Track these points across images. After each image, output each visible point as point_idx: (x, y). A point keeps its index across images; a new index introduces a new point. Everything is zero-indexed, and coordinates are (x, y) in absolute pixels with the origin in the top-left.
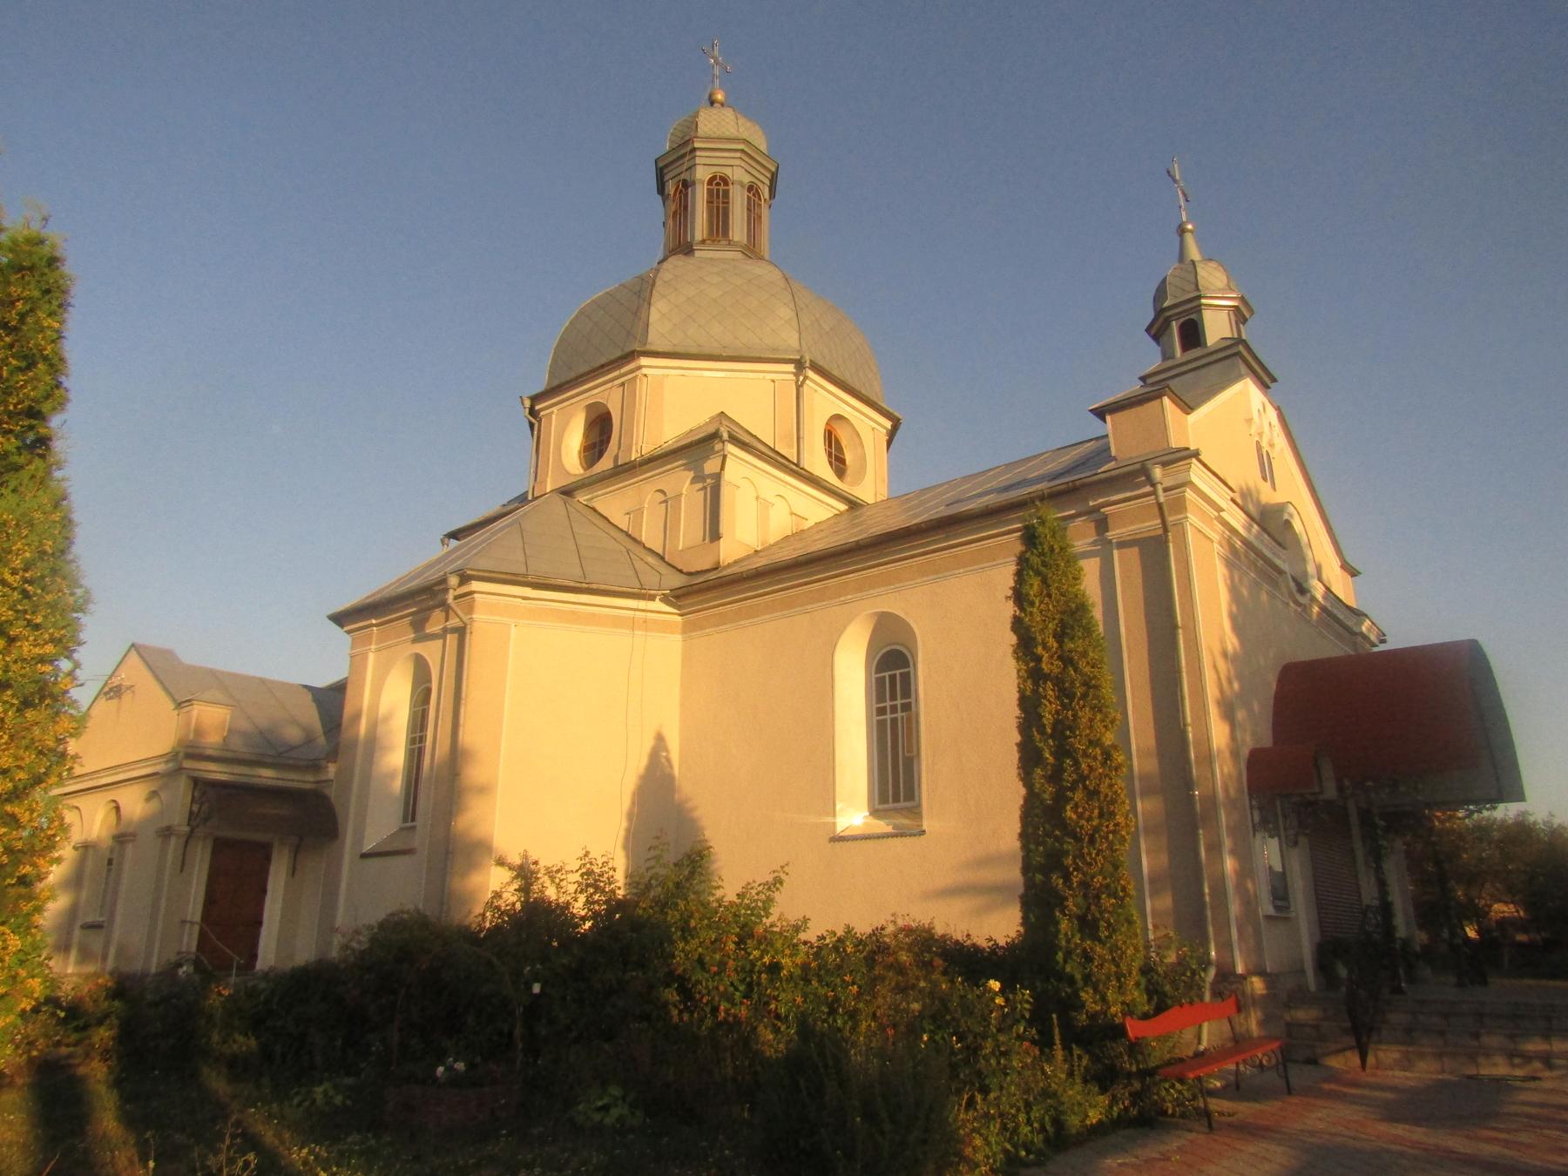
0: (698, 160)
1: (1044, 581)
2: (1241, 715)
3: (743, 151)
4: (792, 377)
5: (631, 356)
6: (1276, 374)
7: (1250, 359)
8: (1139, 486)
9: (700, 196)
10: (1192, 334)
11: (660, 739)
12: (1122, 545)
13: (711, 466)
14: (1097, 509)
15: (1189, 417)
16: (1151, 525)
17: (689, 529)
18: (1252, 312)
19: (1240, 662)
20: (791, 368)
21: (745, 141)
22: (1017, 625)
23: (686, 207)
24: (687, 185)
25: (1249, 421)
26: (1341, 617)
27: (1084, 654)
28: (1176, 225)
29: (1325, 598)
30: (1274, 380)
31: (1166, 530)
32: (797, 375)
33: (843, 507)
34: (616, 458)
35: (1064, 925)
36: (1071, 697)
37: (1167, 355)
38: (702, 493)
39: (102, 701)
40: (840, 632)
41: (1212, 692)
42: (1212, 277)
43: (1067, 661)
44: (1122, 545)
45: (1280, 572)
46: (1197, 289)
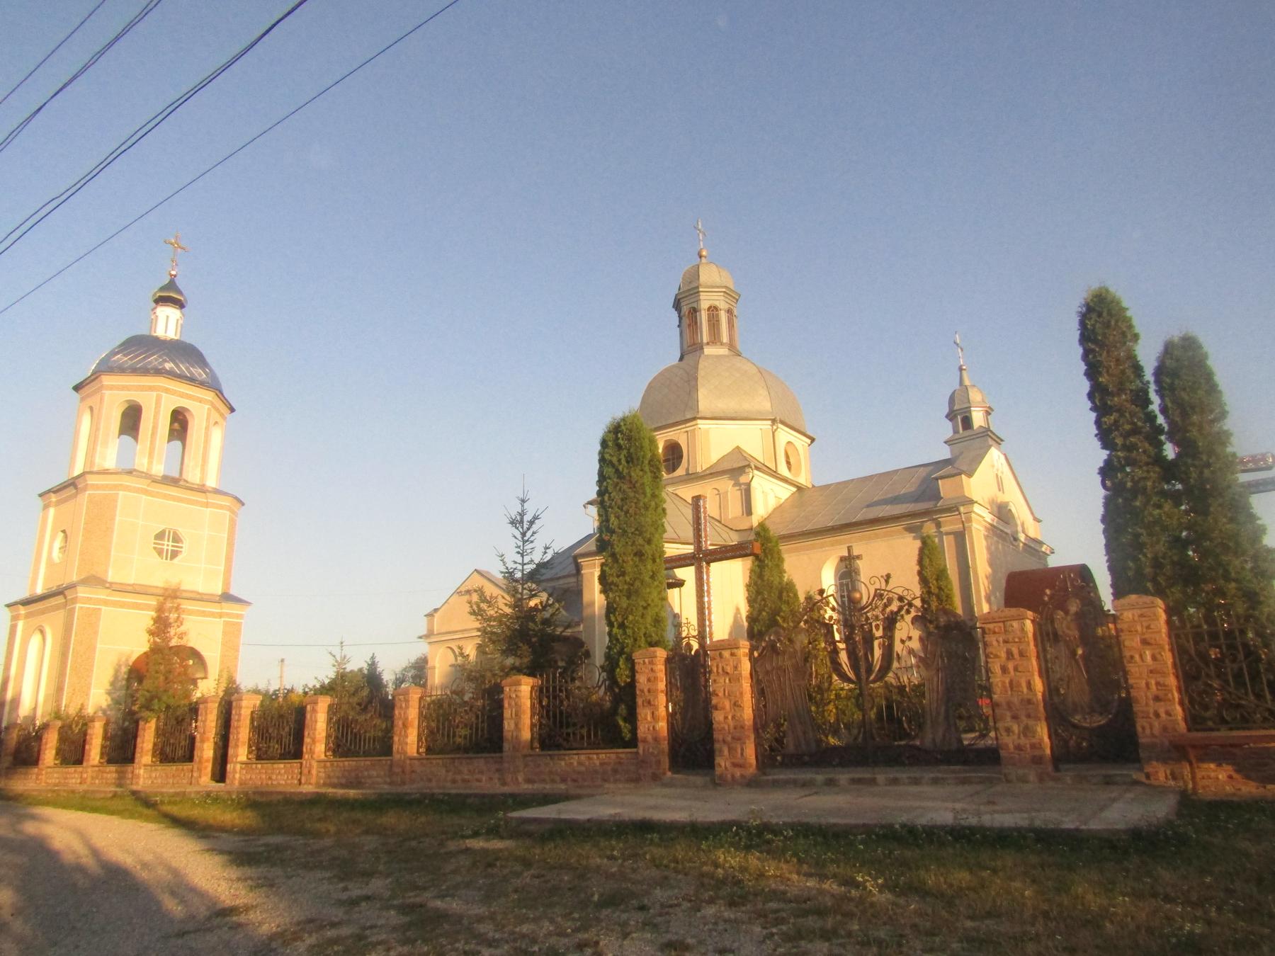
0: (701, 297)
1: (930, 560)
2: (993, 598)
3: (724, 292)
4: (770, 427)
5: (694, 419)
6: (1002, 438)
7: (993, 436)
8: (954, 511)
9: (704, 317)
10: (967, 422)
11: (738, 609)
12: (947, 534)
13: (743, 479)
14: (936, 519)
15: (972, 479)
16: (958, 527)
17: (734, 509)
18: (993, 410)
19: (992, 579)
20: (769, 422)
21: (726, 287)
22: (920, 573)
23: (696, 323)
24: (694, 311)
25: (993, 466)
26: (1033, 545)
27: (946, 587)
28: (957, 368)
29: (1026, 539)
30: (1002, 440)
31: (964, 530)
32: (772, 426)
33: (794, 489)
34: (687, 469)
35: (632, 876)
36: (942, 601)
37: (956, 431)
38: (739, 492)
39: (456, 596)
40: (824, 563)
41: (983, 594)
42: (975, 396)
43: (940, 588)
44: (947, 534)
45: (1007, 534)
46: (969, 402)
